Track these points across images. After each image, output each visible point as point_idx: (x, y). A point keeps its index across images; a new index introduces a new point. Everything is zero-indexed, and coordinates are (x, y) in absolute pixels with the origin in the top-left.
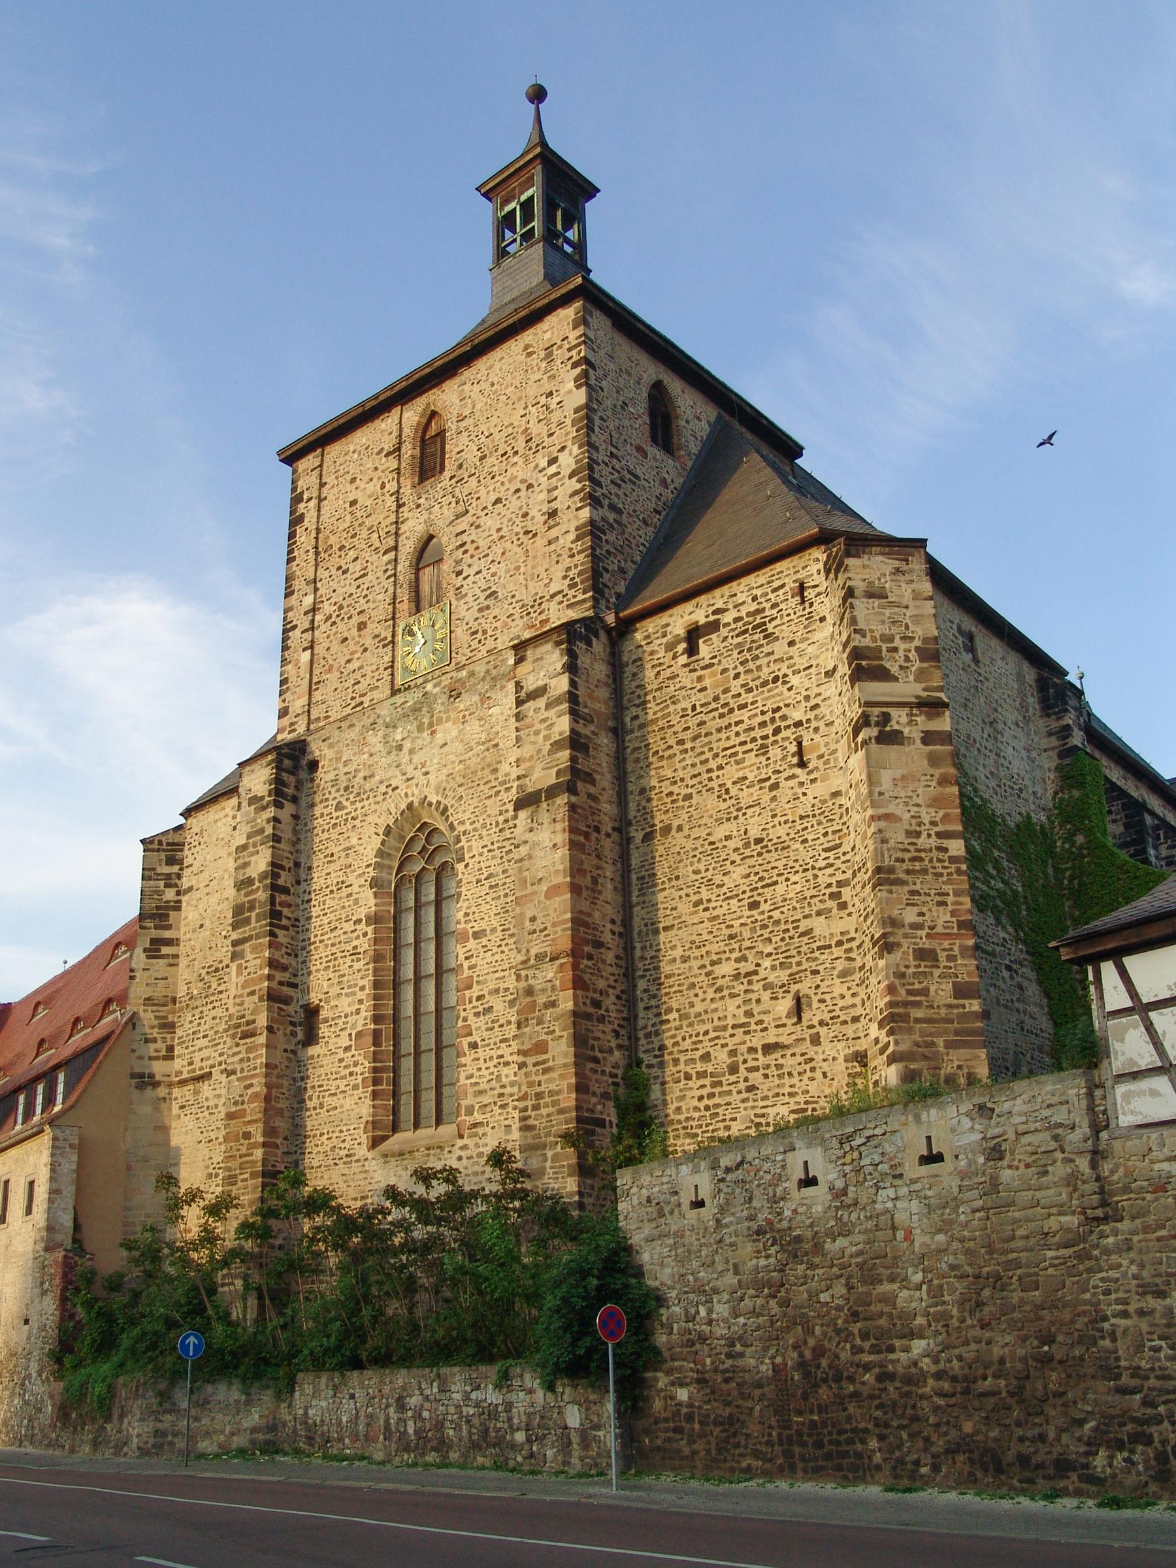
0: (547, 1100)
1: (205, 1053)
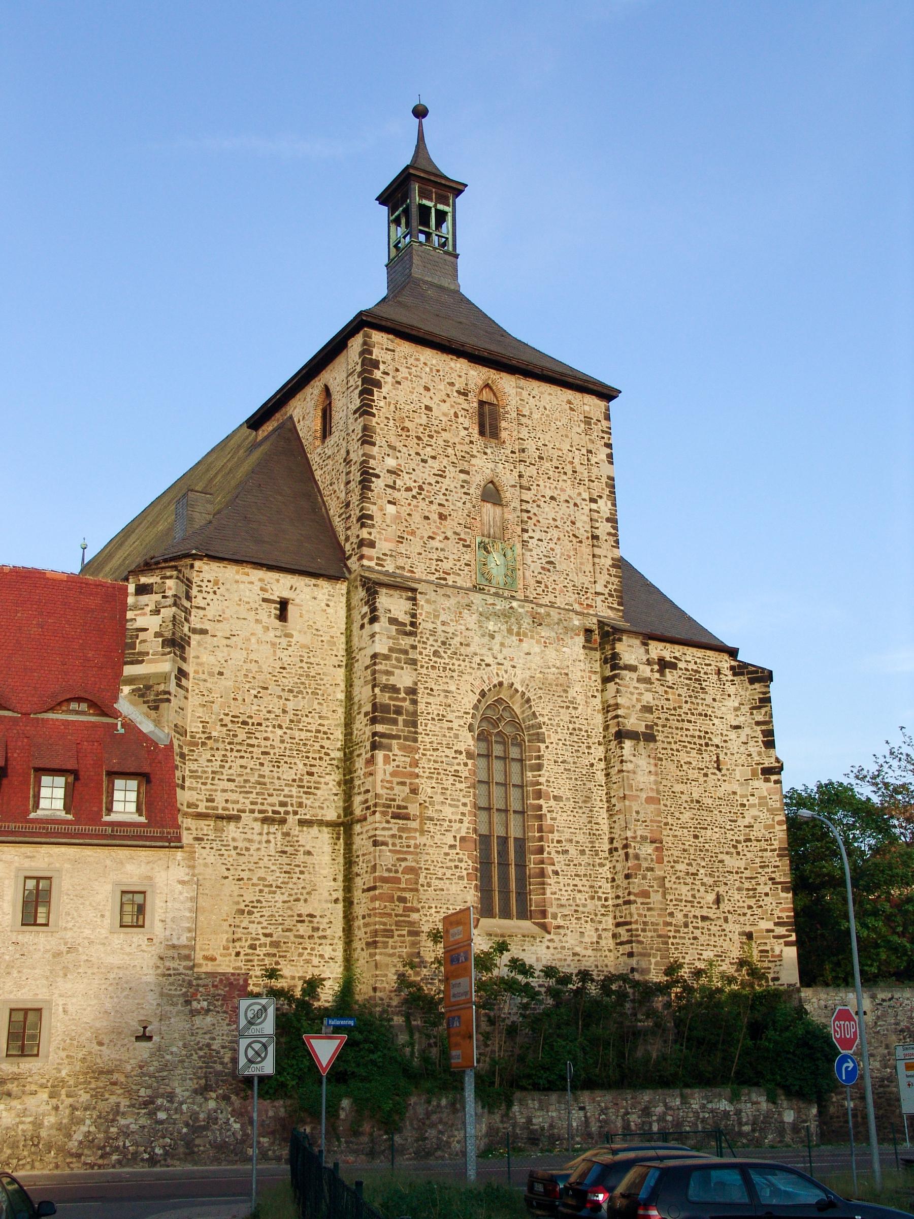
0: (650, 927)
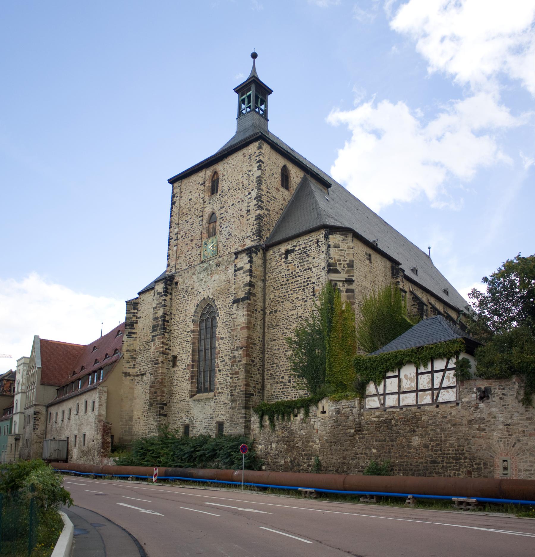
1: (145, 367)
